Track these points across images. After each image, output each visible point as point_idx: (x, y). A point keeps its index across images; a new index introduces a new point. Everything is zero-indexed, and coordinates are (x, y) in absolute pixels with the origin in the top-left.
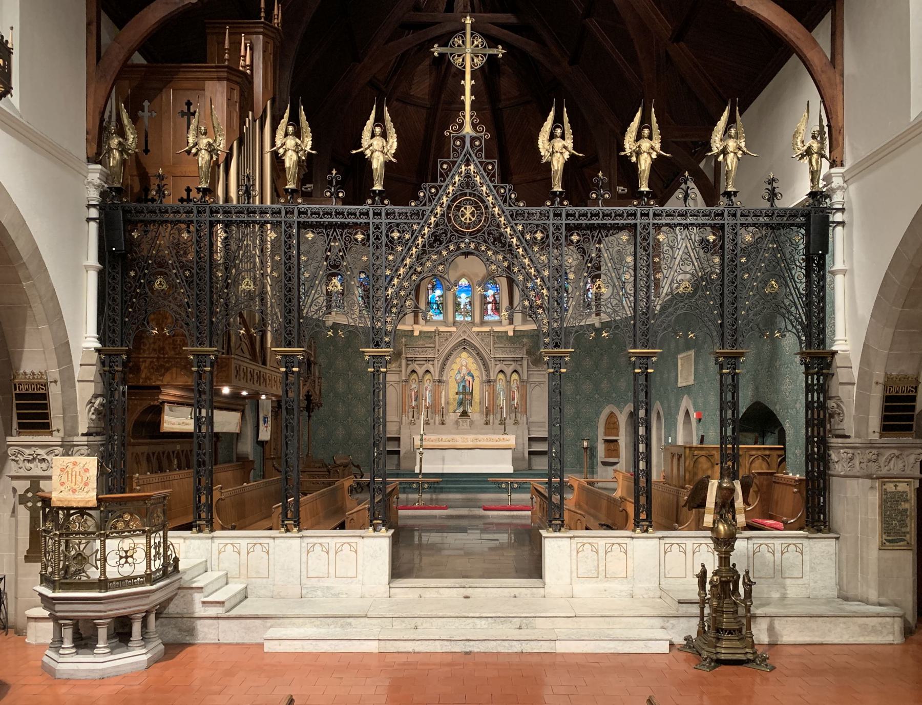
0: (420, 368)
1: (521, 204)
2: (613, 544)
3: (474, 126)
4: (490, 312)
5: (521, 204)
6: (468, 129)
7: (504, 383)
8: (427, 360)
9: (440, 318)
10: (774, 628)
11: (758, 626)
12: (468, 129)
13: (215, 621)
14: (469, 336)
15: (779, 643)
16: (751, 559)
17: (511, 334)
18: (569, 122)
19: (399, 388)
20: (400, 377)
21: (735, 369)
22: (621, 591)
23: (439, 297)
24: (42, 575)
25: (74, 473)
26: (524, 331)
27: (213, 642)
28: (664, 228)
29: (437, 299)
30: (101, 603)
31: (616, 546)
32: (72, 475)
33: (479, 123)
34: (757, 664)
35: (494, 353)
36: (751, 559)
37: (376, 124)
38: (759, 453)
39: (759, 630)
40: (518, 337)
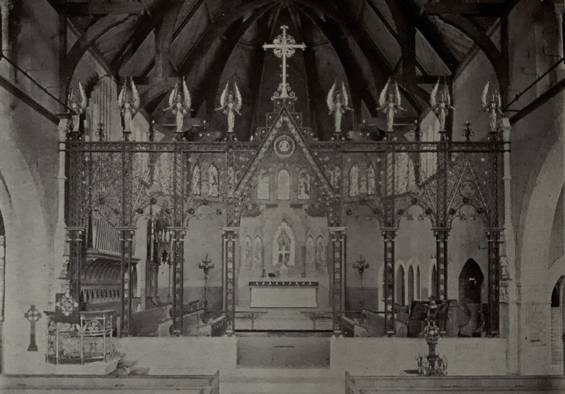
1: (317, 139)
3: (288, 93)
5: (317, 139)
6: (284, 95)
12: (284, 95)
18: (239, 90)
21: (497, 239)
28: (192, 154)
33: (291, 91)
37: (229, 92)
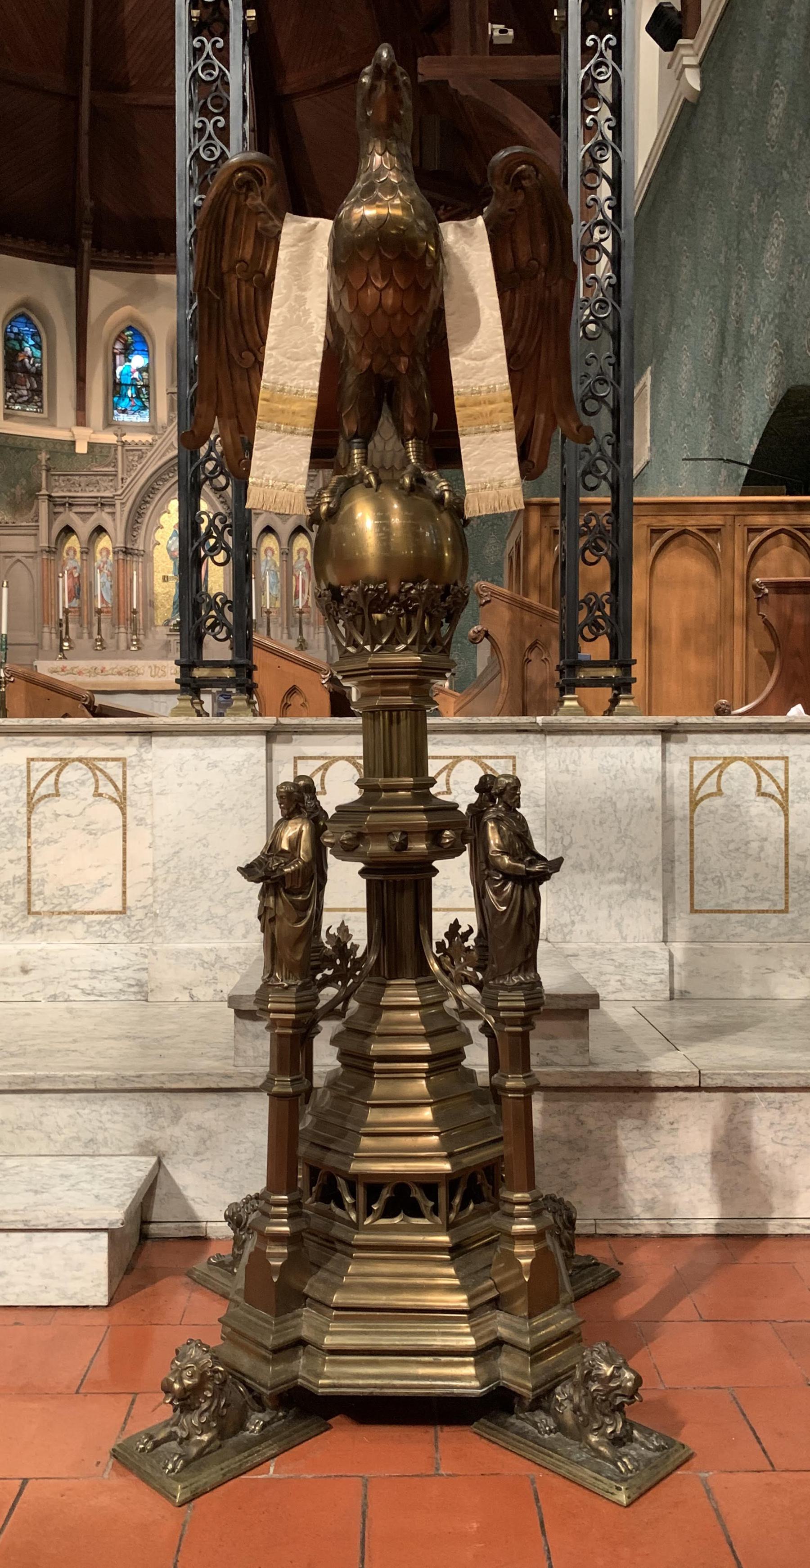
0: (84, 521)
2: (64, 763)
7: (277, 557)
8: (103, 504)
9: (143, 418)
10: (748, 1149)
11: (662, 1138)
15: (773, 1228)
16: (680, 830)
19: (35, 566)
20: (37, 543)
22: (95, 973)
23: (140, 370)
29: (136, 375)
31: (70, 774)
34: (560, 1427)
36: (680, 830)
38: (781, 520)
39: (670, 1159)
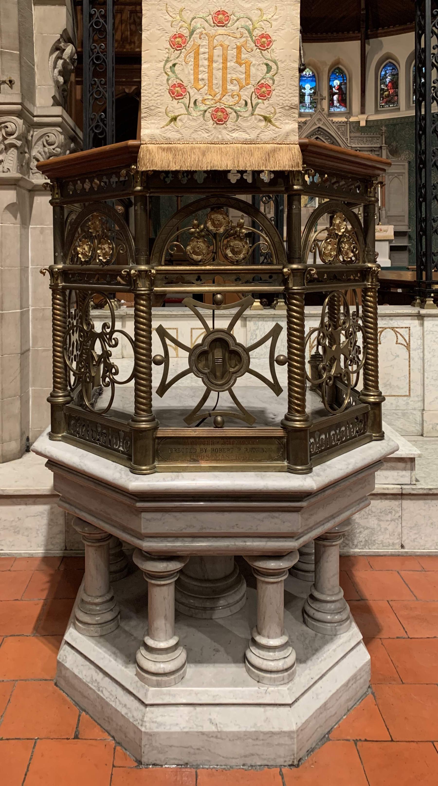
4: (336, 103)
13: (395, 503)
14: (324, 124)
17: (363, 124)
24: (55, 408)
25: (218, 52)
26: (377, 121)
27: (390, 550)
30: (297, 510)
32: (211, 60)
35: (350, 142)
40: (370, 127)
